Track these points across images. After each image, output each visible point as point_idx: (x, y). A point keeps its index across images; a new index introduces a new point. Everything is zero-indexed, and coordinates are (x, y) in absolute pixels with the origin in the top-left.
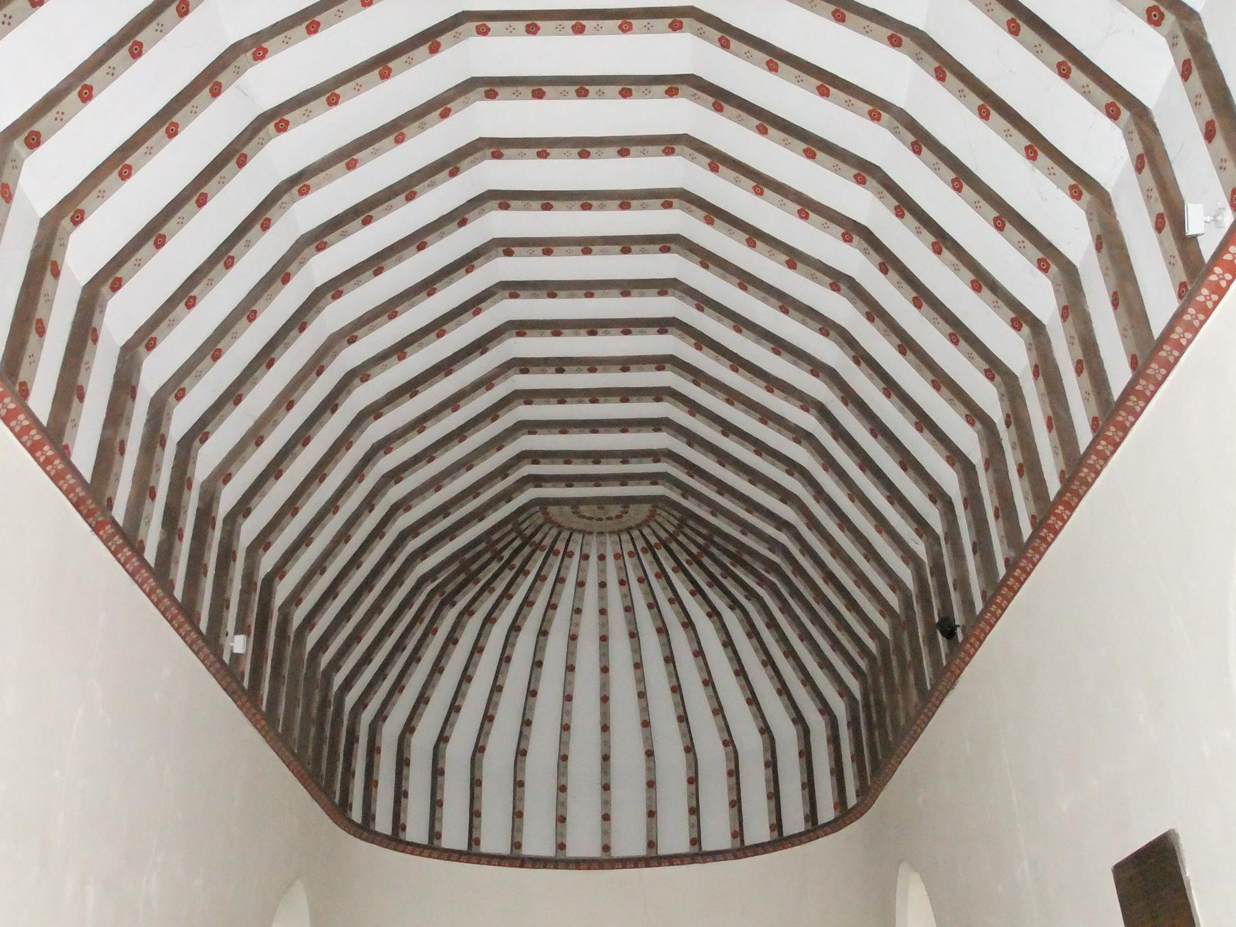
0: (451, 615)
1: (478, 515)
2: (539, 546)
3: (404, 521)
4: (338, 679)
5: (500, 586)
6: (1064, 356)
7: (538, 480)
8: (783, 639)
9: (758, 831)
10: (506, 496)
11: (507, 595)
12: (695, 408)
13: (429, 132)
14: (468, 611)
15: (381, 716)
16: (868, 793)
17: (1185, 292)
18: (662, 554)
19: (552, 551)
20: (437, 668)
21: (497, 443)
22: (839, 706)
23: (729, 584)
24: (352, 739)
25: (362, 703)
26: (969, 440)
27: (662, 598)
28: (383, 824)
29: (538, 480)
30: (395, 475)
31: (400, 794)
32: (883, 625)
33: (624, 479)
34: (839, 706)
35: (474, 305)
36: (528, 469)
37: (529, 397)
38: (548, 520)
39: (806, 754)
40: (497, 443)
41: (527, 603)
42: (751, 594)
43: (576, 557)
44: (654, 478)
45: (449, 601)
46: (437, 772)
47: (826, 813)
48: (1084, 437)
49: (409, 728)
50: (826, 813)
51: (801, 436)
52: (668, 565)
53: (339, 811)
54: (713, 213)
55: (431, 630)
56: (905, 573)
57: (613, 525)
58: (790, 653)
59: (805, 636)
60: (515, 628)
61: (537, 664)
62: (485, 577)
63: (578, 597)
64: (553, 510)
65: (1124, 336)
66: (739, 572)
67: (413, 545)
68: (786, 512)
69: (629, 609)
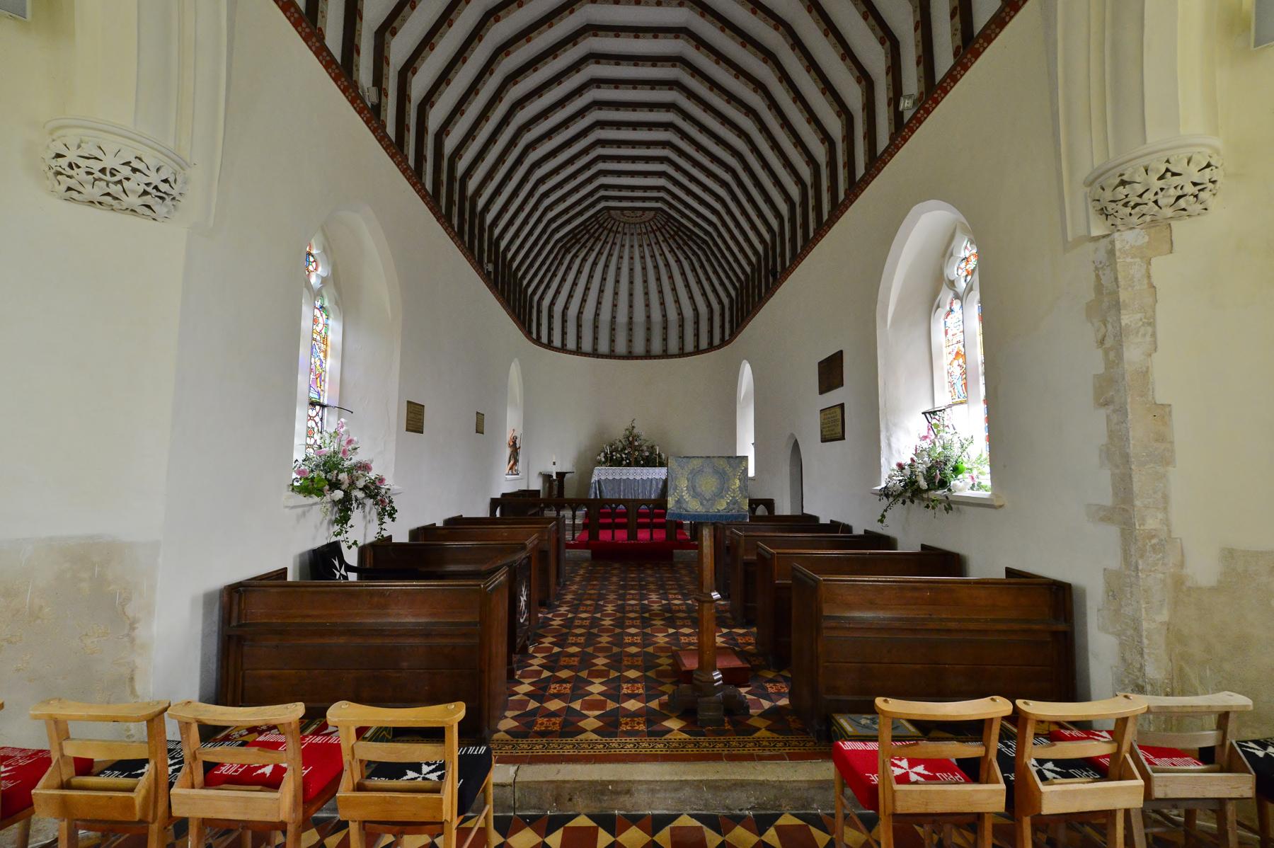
0: (569, 257)
1: (581, 213)
2: (605, 228)
3: (551, 215)
4: (525, 283)
5: (589, 245)
6: (841, 159)
7: (607, 198)
8: (706, 273)
9: (689, 347)
10: (592, 205)
11: (591, 249)
12: (678, 168)
13: (565, 21)
14: (576, 256)
15: (541, 298)
16: (733, 335)
17: (893, 138)
18: (658, 233)
19: (610, 230)
20: (563, 280)
21: (590, 180)
22: (726, 301)
23: (685, 248)
24: (531, 307)
25: (534, 292)
26: (794, 192)
27: (657, 254)
28: (544, 340)
29: (607, 198)
30: (546, 195)
31: (550, 329)
32: (748, 269)
33: (644, 199)
34: (726, 301)
35: (581, 113)
36: (602, 193)
37: (604, 158)
38: (610, 216)
39: (711, 320)
40: (590, 180)
41: (600, 253)
42: (695, 253)
43: (627, 247)
44: (657, 199)
45: (568, 251)
46: (579, 326)
47: (717, 341)
48: (842, 196)
49: (552, 303)
50: (717, 341)
51: (724, 184)
52: (661, 238)
53: (528, 334)
54: (696, 72)
55: (561, 263)
56: (760, 248)
57: (638, 220)
58: (709, 279)
59: (715, 272)
60: (606, 266)
61: (616, 294)
62: (583, 241)
63: (621, 251)
64: (612, 212)
65: (917, 46)
66: (690, 243)
67: (554, 226)
68: (714, 218)
69: (643, 257)
